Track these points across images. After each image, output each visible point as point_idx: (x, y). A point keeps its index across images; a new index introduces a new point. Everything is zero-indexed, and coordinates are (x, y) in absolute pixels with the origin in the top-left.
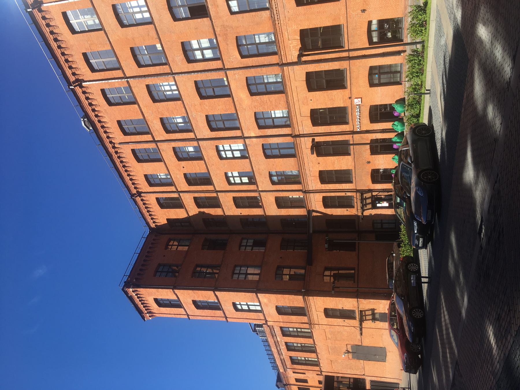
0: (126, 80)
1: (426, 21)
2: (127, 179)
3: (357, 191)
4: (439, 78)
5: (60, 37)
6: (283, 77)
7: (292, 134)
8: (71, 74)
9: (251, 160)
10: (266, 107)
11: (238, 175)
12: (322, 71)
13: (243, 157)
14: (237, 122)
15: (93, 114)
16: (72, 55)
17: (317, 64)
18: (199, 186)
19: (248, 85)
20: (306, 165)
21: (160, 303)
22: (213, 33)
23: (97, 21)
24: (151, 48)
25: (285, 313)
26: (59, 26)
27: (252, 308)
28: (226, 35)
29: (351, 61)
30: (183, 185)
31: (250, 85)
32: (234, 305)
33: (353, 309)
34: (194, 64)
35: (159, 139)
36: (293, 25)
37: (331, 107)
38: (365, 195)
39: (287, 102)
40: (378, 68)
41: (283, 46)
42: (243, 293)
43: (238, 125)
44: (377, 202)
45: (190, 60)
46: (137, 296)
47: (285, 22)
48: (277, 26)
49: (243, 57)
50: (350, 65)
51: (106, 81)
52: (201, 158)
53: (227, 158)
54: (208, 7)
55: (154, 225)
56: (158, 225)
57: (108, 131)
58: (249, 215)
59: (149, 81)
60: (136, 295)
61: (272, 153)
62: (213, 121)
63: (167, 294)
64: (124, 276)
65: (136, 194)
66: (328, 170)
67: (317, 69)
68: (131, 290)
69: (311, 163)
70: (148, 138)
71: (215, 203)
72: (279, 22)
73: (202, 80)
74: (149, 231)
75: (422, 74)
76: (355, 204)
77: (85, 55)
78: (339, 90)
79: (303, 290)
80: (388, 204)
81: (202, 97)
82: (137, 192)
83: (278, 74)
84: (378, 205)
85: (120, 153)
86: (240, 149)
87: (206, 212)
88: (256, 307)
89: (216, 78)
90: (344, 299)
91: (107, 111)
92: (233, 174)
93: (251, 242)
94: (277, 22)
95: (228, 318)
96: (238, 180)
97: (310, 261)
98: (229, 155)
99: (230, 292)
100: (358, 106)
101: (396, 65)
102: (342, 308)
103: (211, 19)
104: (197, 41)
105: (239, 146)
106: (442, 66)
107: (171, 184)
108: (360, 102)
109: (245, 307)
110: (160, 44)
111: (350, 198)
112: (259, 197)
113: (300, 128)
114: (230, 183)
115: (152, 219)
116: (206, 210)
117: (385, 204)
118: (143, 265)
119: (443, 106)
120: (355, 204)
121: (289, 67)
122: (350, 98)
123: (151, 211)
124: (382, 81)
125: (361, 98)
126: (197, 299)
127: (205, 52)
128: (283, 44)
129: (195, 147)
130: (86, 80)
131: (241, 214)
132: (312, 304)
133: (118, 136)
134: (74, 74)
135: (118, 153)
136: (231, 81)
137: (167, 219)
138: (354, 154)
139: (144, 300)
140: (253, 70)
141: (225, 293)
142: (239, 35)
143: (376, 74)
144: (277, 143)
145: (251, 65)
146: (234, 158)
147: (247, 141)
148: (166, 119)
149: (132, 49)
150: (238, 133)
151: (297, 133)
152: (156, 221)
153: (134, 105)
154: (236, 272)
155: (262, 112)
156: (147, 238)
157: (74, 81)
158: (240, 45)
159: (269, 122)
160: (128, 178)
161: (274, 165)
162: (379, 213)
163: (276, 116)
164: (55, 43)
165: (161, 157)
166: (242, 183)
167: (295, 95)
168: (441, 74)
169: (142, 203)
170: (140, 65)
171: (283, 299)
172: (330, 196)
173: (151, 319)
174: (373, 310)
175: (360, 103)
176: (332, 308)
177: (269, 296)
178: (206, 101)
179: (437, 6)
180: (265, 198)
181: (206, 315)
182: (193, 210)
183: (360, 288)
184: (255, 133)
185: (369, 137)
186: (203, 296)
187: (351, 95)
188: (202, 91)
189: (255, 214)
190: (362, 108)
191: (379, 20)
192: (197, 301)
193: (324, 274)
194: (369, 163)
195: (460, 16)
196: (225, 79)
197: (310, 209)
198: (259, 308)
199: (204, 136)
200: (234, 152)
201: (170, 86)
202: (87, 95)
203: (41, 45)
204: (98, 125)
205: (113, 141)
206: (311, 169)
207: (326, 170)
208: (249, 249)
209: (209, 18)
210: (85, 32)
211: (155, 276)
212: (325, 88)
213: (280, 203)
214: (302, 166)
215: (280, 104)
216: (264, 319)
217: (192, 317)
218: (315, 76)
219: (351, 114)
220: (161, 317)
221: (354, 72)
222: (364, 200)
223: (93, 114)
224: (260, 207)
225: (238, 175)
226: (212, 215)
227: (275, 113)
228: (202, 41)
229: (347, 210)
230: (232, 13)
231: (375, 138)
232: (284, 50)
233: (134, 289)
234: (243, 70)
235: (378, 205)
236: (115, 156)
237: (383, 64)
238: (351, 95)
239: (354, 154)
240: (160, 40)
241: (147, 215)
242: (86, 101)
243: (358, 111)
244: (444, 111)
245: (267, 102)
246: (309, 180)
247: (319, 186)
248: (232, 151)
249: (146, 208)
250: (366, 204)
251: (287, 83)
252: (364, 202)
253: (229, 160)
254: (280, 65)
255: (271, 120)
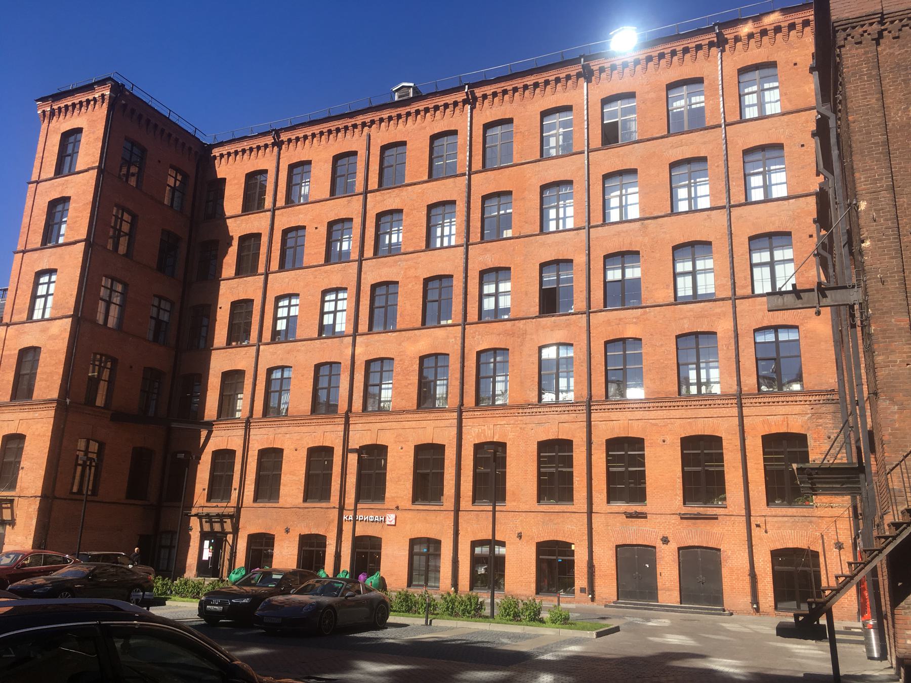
0: (467, 173)
1: (520, 621)
2: (309, 131)
3: (239, 509)
4: (457, 636)
5: (539, 92)
6: (442, 410)
7: (351, 411)
8: (485, 93)
9: (316, 341)
10: (400, 377)
11: (291, 315)
12: (444, 469)
13: (322, 328)
14: (381, 329)
15: (421, 108)
16: (512, 102)
17: (455, 463)
18: (279, 247)
19: (436, 355)
20: (297, 428)
21: (70, 138)
22: (518, 316)
23: (553, 152)
24: (506, 222)
25: (22, 361)
26: (555, 96)
27: (40, 303)
28: (513, 334)
29: (452, 513)
30: (285, 219)
31: (437, 358)
32: (51, 272)
33: (17, 487)
34: (477, 280)
35: (368, 200)
36: (514, 434)
37: (387, 478)
38: (229, 521)
39: (404, 411)
40: (437, 553)
41: (486, 416)
42: (75, 293)
43: (375, 330)
44: (213, 541)
45: (485, 275)
46: (92, 100)
47: (519, 422)
48: (515, 411)
49: (479, 354)
50: (447, 512)
51: (468, 143)
52: (328, 260)
53: (323, 302)
54: (553, 316)
55: (217, 154)
56: (216, 161)
57: (392, 122)
58: (216, 320)
59: (461, 207)
60: (95, 98)
61: (323, 376)
62: (387, 291)
63: (89, 155)
64: (133, 85)
65: (278, 140)
66: (283, 464)
67: (447, 462)
68: (107, 93)
69: (298, 438)
70: (373, 183)
71: (246, 267)
72: (520, 415)
73: (452, 286)
74: (206, 144)
75: (449, 615)
76: (215, 504)
77: (510, 121)
78: (411, 492)
79: (68, 401)
80: (207, 559)
81: (427, 281)
82: (282, 142)
83: (447, 403)
84: (207, 543)
85: (354, 132)
86: (337, 326)
87: (231, 249)
88: (41, 311)
89: (453, 308)
90: (43, 473)
91: (423, 131)
92: (294, 307)
93: (165, 317)
94: (521, 411)
95: (23, 256)
96: (282, 312)
97: (119, 417)
98: (329, 307)
99: (80, 270)
100: (383, 519)
101: (437, 579)
102: (22, 468)
103: (536, 317)
104: (510, 291)
105: (342, 324)
106: (479, 639)
107: (290, 201)
108: (389, 523)
109: (42, 290)
110: (511, 236)
111: (227, 496)
112: (248, 343)
113: (359, 427)
114: (278, 299)
115: (229, 154)
116: (233, 250)
117: (207, 555)
118: (148, 121)
119: (427, 640)
120: (215, 504)
121: (456, 421)
122: (397, 508)
123: (243, 155)
124: (416, 558)
125: (395, 525)
126: (72, 206)
127: (493, 299)
128: (489, 416)
129: (348, 253)
130: (474, 112)
131: (220, 308)
132: (37, 415)
133: (383, 135)
134: (485, 97)
135: (354, 129)
136: (447, 330)
137: (225, 179)
138: (306, 508)
139: (80, 110)
140: (459, 366)
141: (81, 260)
142: (510, 354)
143: (428, 550)
144: (339, 387)
145: (465, 364)
146: (322, 313)
147: (350, 339)
148: (400, 218)
149: (509, 193)
150: (363, 327)
151: (352, 421)
152: (223, 160)
153: (427, 175)
154: (163, 302)
155: (392, 371)
156: (194, 136)
157: (475, 94)
158: (495, 353)
159: (375, 379)
160: (309, 134)
161: (302, 376)
162: (191, 544)
163: (382, 391)
164: (532, 83)
165: (336, 196)
166: (276, 319)
167: (413, 424)
168: (464, 638)
169: (262, 144)
170: (485, 198)
171: (54, 362)
172: (234, 462)
173: (39, 112)
174: (12, 523)
175: (388, 523)
176: (25, 448)
177: (63, 339)
178: (420, 287)
179: (543, 635)
180: (246, 354)
181: (33, 216)
182: (237, 227)
183: (85, 505)
184: (360, 354)
185: (331, 534)
186: (78, 219)
187: (402, 510)
188: (436, 284)
189: (216, 332)
190: (381, 525)
191: (505, 557)
192: (66, 204)
193: (91, 441)
194: (287, 531)
195: (549, 658)
196: (450, 322)
197: (215, 426)
198: (37, 315)
199: (365, 273)
200: (332, 316)
201: (450, 236)
202: (451, 107)
203: (530, 61)
204: (403, 111)
205: (374, 126)
206: (288, 435)
207: (283, 461)
208: (154, 312)
209: (537, 314)
210: (542, 132)
211: (127, 139)
212: (418, 471)
213: (233, 379)
214: (295, 422)
215: (402, 399)
216: (12, 321)
217: (34, 189)
218: (437, 457)
219: (372, 507)
220: (40, 131)
221: (436, 517)
222: (219, 520)
223: (421, 108)
224: (229, 343)
225: (291, 314)
226: (224, 258)
227: (388, 389)
228: (509, 298)
229: (204, 490)
230: (540, 349)
231: (327, 543)
232: (481, 416)
233: (107, 97)
234: (459, 351)
235: (207, 543)
236: (350, 122)
237: (442, 560)
238: (402, 510)
239: (306, 508)
240: (517, 238)
241: (239, 146)
242: (442, 103)
243: (376, 519)
244: (422, 642)
245: (407, 379)
246: (269, 432)
247: (256, 445)
248: (335, 312)
249: (251, 149)
250: (211, 523)
251: (433, 415)
252: (216, 520)
253: (319, 304)
254: (460, 408)
255: (378, 382)
